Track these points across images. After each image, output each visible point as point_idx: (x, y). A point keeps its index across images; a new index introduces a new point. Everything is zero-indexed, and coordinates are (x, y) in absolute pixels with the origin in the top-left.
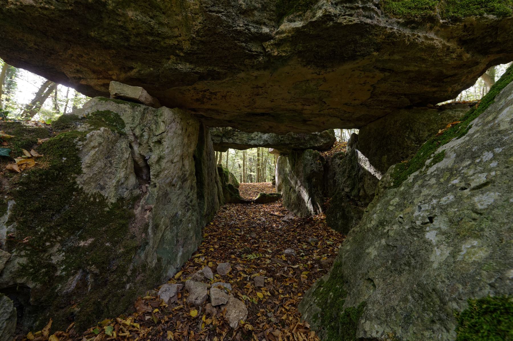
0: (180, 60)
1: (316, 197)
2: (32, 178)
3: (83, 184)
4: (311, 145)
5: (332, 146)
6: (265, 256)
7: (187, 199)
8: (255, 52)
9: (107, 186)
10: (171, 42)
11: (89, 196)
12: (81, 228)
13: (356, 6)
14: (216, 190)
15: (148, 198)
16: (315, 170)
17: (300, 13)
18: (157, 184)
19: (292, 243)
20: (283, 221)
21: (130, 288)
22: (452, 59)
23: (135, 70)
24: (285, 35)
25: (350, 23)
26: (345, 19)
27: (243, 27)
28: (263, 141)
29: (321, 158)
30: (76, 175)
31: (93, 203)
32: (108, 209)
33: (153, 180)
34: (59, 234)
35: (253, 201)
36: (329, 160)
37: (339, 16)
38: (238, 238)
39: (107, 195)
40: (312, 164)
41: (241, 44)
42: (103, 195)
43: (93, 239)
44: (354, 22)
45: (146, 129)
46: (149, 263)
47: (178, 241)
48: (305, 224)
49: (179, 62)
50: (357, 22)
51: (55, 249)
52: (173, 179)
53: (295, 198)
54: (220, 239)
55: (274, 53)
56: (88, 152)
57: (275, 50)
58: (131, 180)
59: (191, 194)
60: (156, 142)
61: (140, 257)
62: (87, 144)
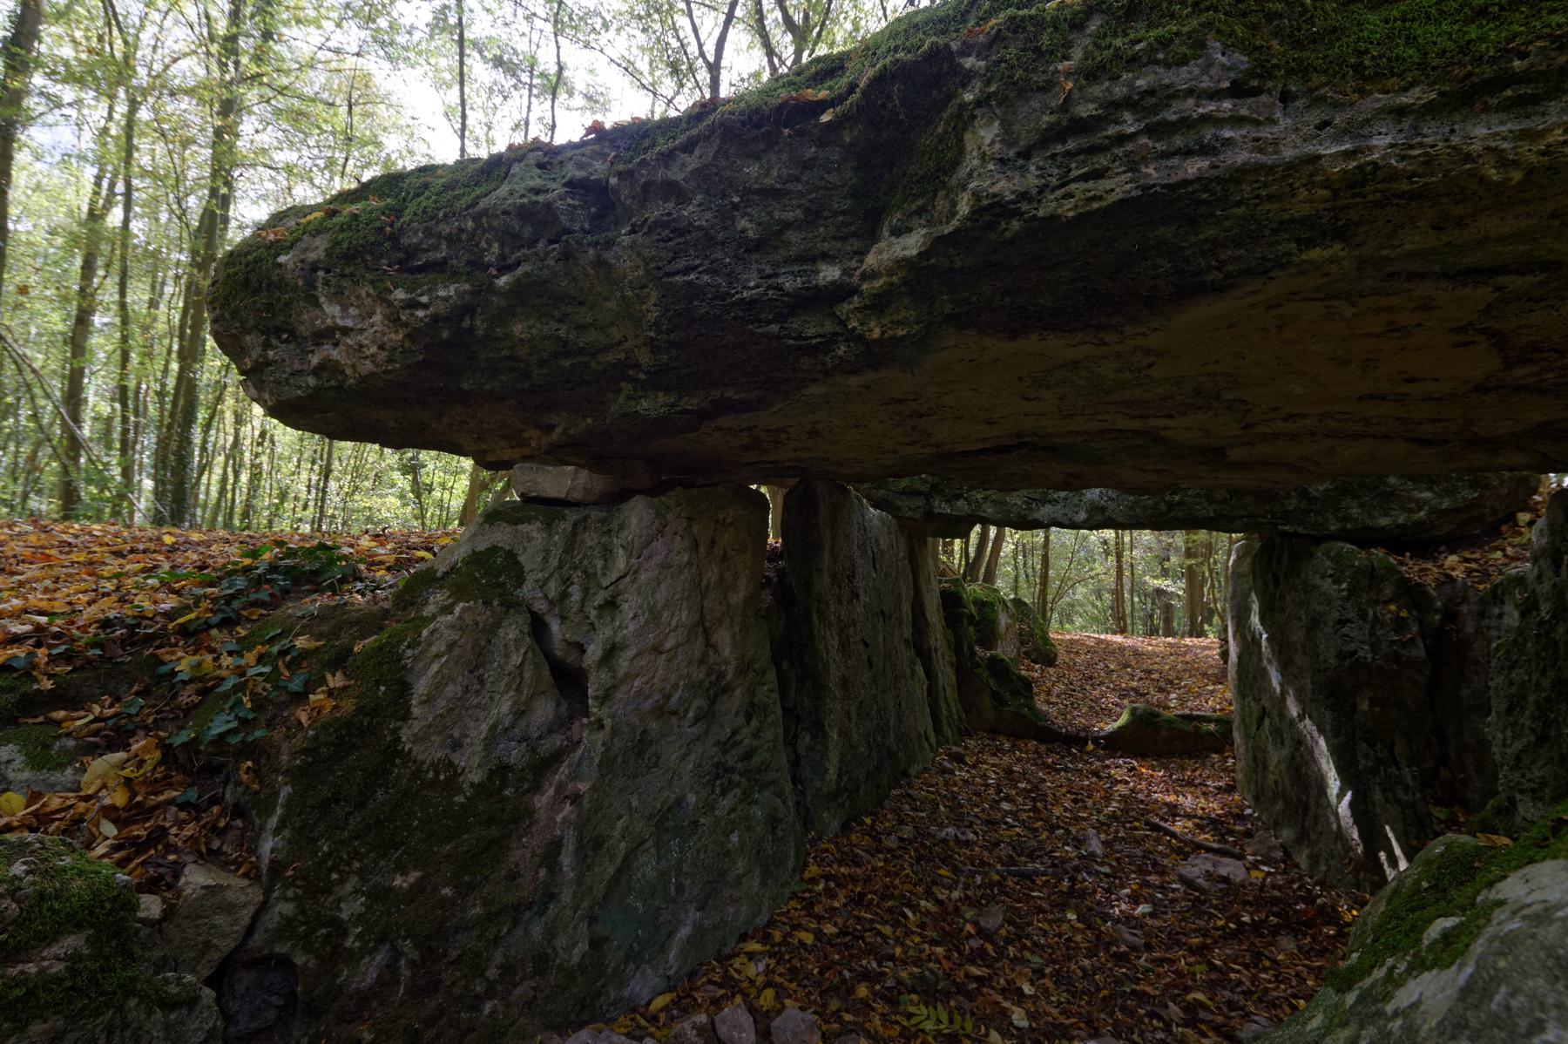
0: (643, 388)
1: (1378, 796)
2: (322, 738)
3: (413, 742)
4: (1346, 519)
5: (1511, 518)
6: (987, 1035)
7: (725, 752)
8: (815, 337)
9: (468, 740)
10: (610, 358)
11: (425, 767)
12: (402, 843)
13: (1107, 137)
14: (919, 686)
15: (580, 759)
16: (1365, 653)
17: (920, 202)
18: (608, 722)
19: (1152, 1015)
20: (1183, 880)
21: (492, 1013)
22: (1317, 490)
23: (558, 430)
24: (881, 282)
25: (1095, 205)
26: (1070, 195)
27: (757, 286)
28: (1087, 511)
29: (1412, 594)
30: (399, 724)
31: (433, 784)
32: (462, 799)
33: (595, 710)
34: (357, 855)
35: (1096, 741)
36: (1465, 609)
37: (1040, 192)
38: (928, 913)
39: (463, 764)
40: (1342, 622)
41: (766, 329)
42: (456, 762)
43: (418, 874)
44: (1112, 198)
45: (577, 577)
46: (561, 952)
47: (680, 888)
48: (1276, 931)
49: (640, 394)
50: (1121, 196)
51: (349, 887)
52: (668, 697)
53: (1283, 766)
54: (858, 901)
55: (871, 331)
56: (426, 667)
57: (872, 324)
58: (540, 712)
59: (746, 732)
60: (601, 607)
61: (527, 932)
62: (421, 652)
